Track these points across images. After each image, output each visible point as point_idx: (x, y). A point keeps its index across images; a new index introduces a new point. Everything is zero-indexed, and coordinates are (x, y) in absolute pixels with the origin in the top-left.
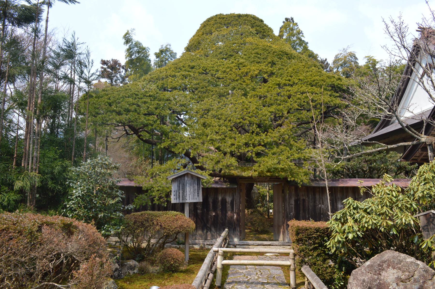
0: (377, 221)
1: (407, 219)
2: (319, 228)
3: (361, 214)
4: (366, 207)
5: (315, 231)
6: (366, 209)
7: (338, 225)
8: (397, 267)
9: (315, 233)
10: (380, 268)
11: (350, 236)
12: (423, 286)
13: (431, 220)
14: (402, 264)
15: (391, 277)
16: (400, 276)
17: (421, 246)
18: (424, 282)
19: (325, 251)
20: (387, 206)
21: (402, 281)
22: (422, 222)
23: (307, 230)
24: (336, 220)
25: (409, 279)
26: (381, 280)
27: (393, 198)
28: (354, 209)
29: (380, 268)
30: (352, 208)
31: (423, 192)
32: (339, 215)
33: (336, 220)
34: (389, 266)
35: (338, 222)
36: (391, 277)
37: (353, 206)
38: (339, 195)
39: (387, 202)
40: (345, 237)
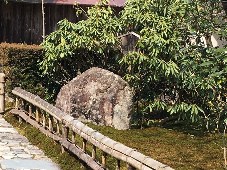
0: (86, 41)
1: (111, 38)
2: (33, 50)
3: (73, 35)
4: (79, 28)
5: (28, 53)
6: (78, 30)
7: (52, 46)
8: (98, 80)
9: (28, 55)
10: (85, 82)
11: (62, 55)
12: (116, 95)
13: (131, 40)
14: (102, 77)
15: (92, 89)
16: (99, 88)
17: (119, 62)
18: (117, 92)
19: (37, 74)
20: (97, 28)
21: (101, 92)
22: (124, 41)
23: (20, 52)
24: (50, 41)
25: (106, 90)
26: (84, 92)
27: (103, 20)
28: (68, 30)
29: (85, 82)
30: (66, 29)
31: (127, 15)
32: (53, 36)
33: (50, 41)
34: (92, 79)
35: (52, 44)
36: (92, 89)
37: (67, 28)
38: (56, 15)
39: (98, 24)
40: (57, 56)
